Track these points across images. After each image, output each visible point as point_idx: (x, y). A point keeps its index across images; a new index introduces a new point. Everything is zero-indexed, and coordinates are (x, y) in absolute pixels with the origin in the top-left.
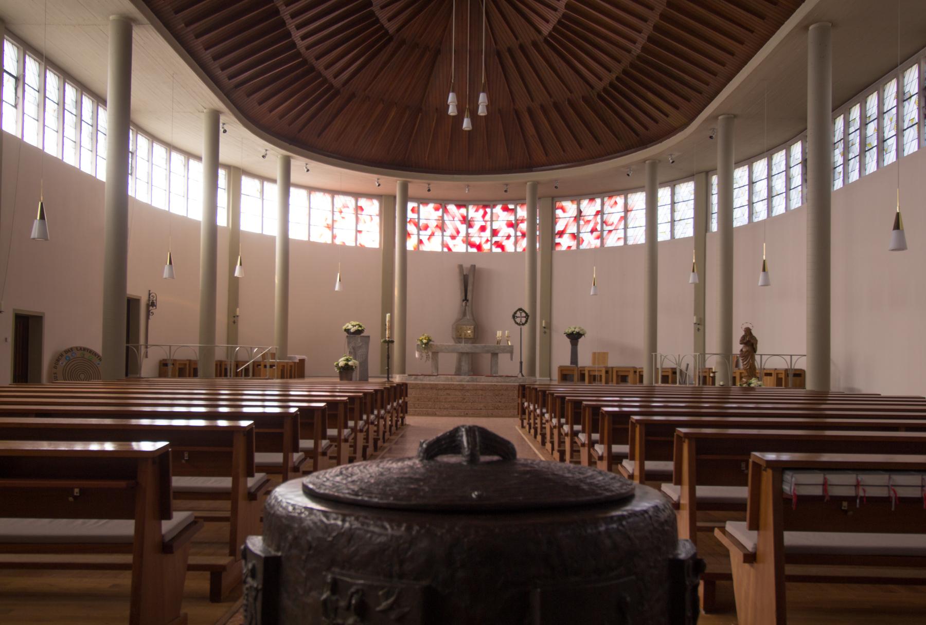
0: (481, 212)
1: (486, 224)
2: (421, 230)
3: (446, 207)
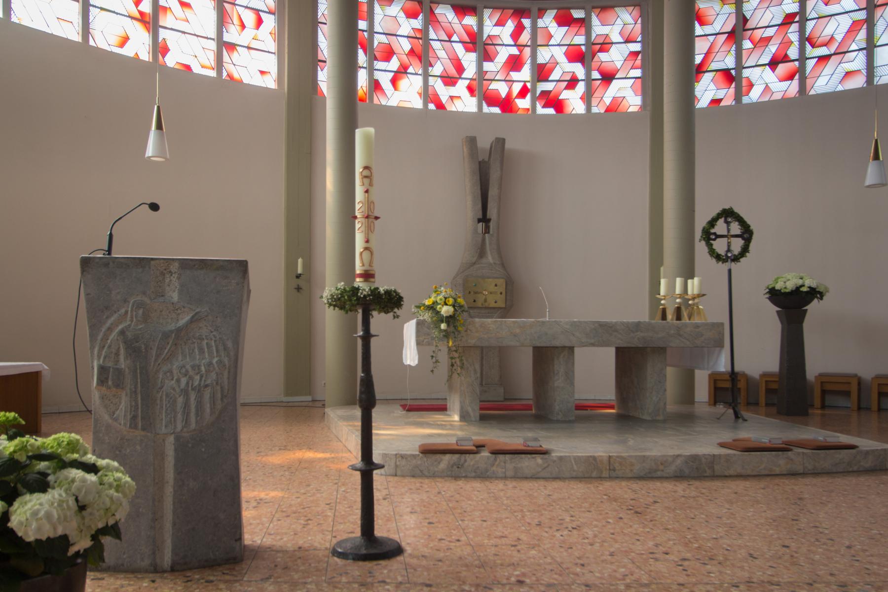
0: (510, 26)
1: (521, 51)
2: (376, 59)
3: (432, 12)
